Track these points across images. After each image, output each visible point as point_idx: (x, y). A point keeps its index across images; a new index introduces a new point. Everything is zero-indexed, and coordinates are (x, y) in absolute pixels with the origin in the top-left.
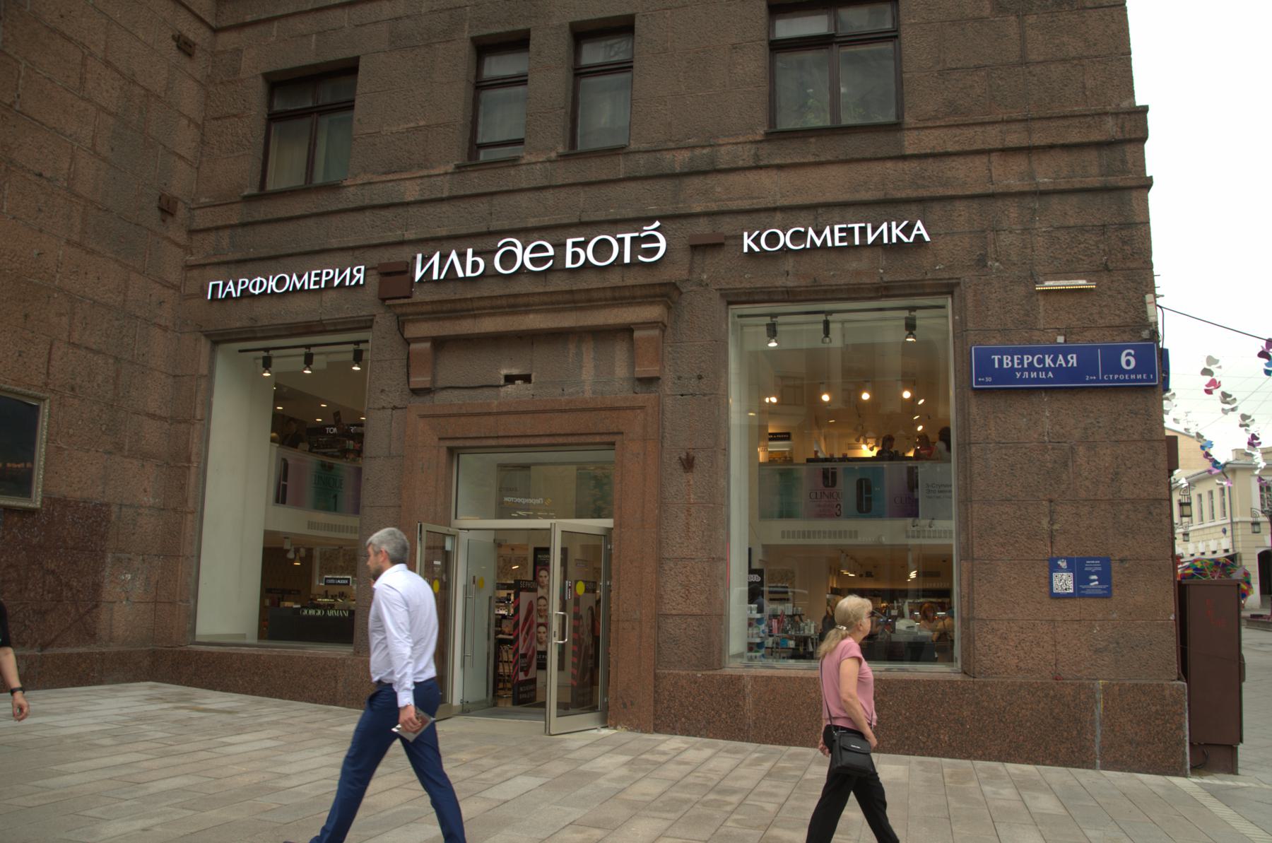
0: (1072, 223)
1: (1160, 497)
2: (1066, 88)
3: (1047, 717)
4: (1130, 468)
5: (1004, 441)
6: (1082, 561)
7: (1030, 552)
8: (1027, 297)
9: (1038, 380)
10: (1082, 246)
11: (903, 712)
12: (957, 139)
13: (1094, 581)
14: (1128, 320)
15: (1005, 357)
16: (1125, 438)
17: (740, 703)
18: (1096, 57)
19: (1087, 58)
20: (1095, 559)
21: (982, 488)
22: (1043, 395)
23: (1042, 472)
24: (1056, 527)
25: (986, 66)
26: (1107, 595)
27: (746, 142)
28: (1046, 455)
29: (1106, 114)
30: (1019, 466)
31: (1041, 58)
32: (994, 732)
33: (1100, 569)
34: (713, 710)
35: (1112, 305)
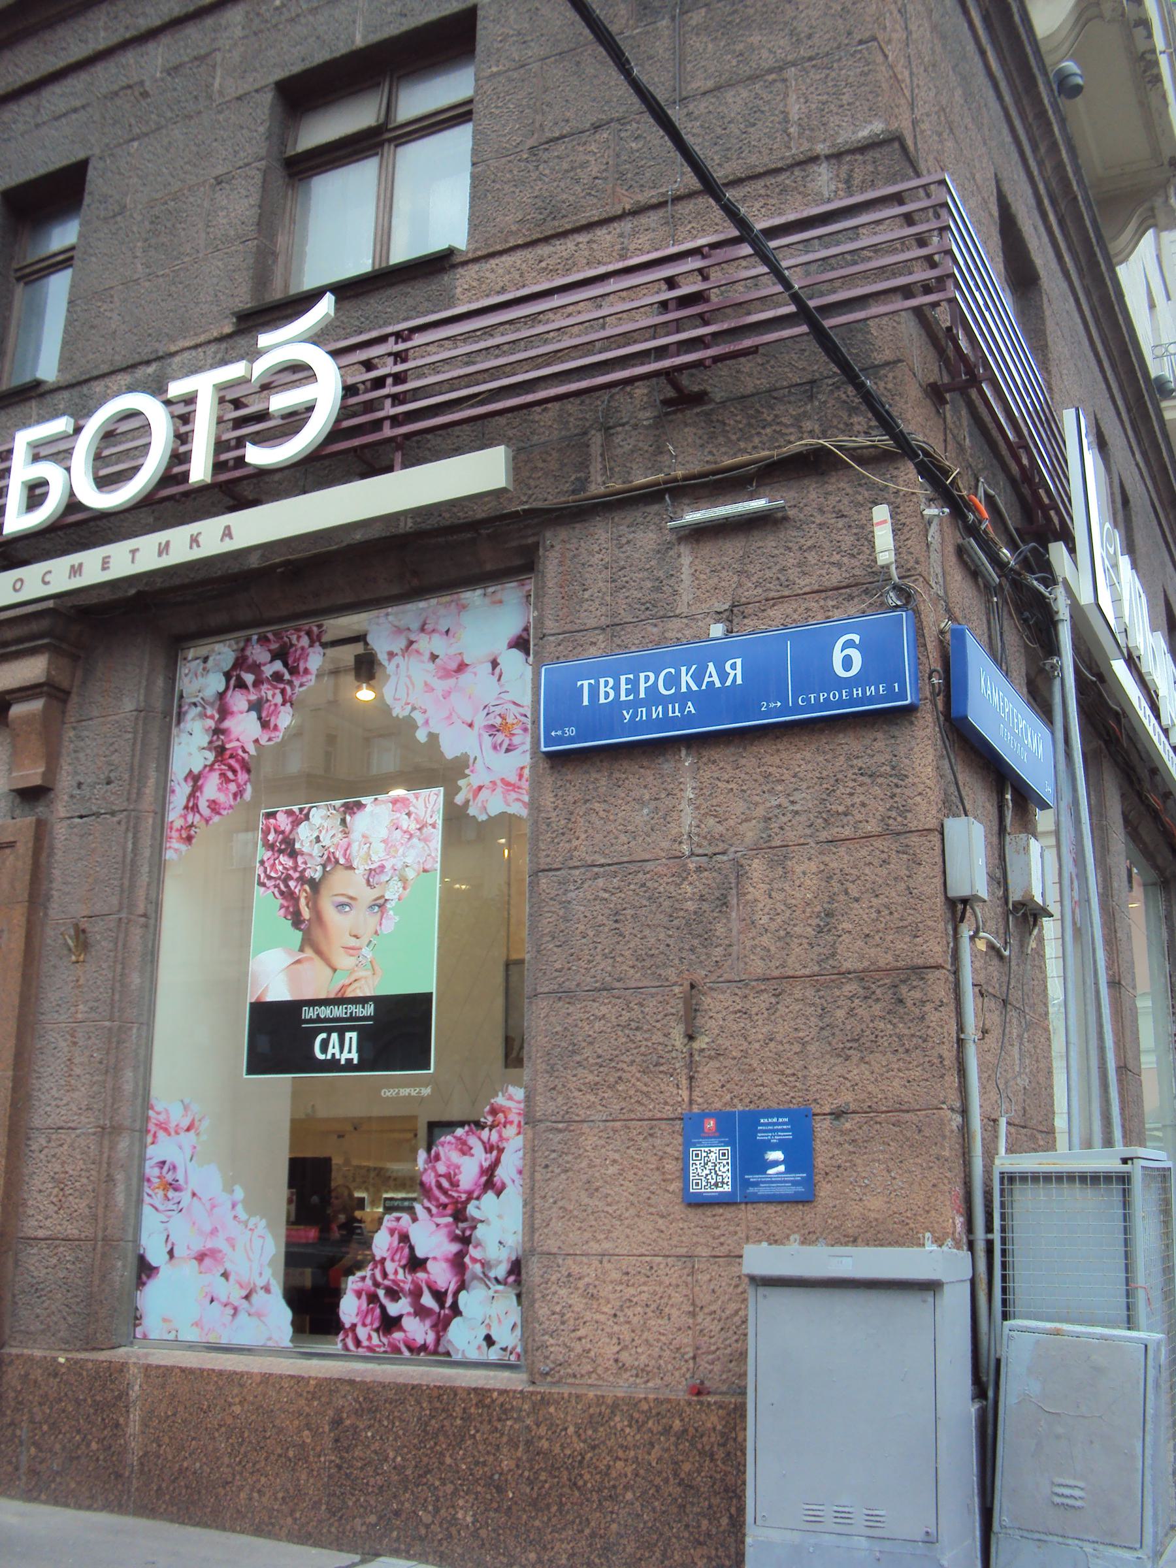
0: (750, 389)
1: (920, 962)
2: (752, 130)
3: (666, 1480)
4: (857, 900)
5: (603, 861)
6: (751, 1120)
7: (645, 1101)
8: (659, 552)
9: (666, 723)
10: (768, 430)
11: (391, 1455)
12: (543, 264)
13: (776, 1163)
14: (857, 572)
15: (602, 681)
16: (847, 832)
17: (121, 1420)
18: (811, 59)
19: (794, 64)
20: (779, 1113)
21: (558, 966)
22: (683, 753)
23: (676, 922)
24: (701, 1043)
25: (612, 120)
26: (805, 1200)
27: (209, 342)
28: (685, 885)
29: (814, 159)
30: (629, 912)
31: (710, 84)
32: (560, 1510)
33: (788, 1136)
34: (79, 1432)
35: (827, 544)
